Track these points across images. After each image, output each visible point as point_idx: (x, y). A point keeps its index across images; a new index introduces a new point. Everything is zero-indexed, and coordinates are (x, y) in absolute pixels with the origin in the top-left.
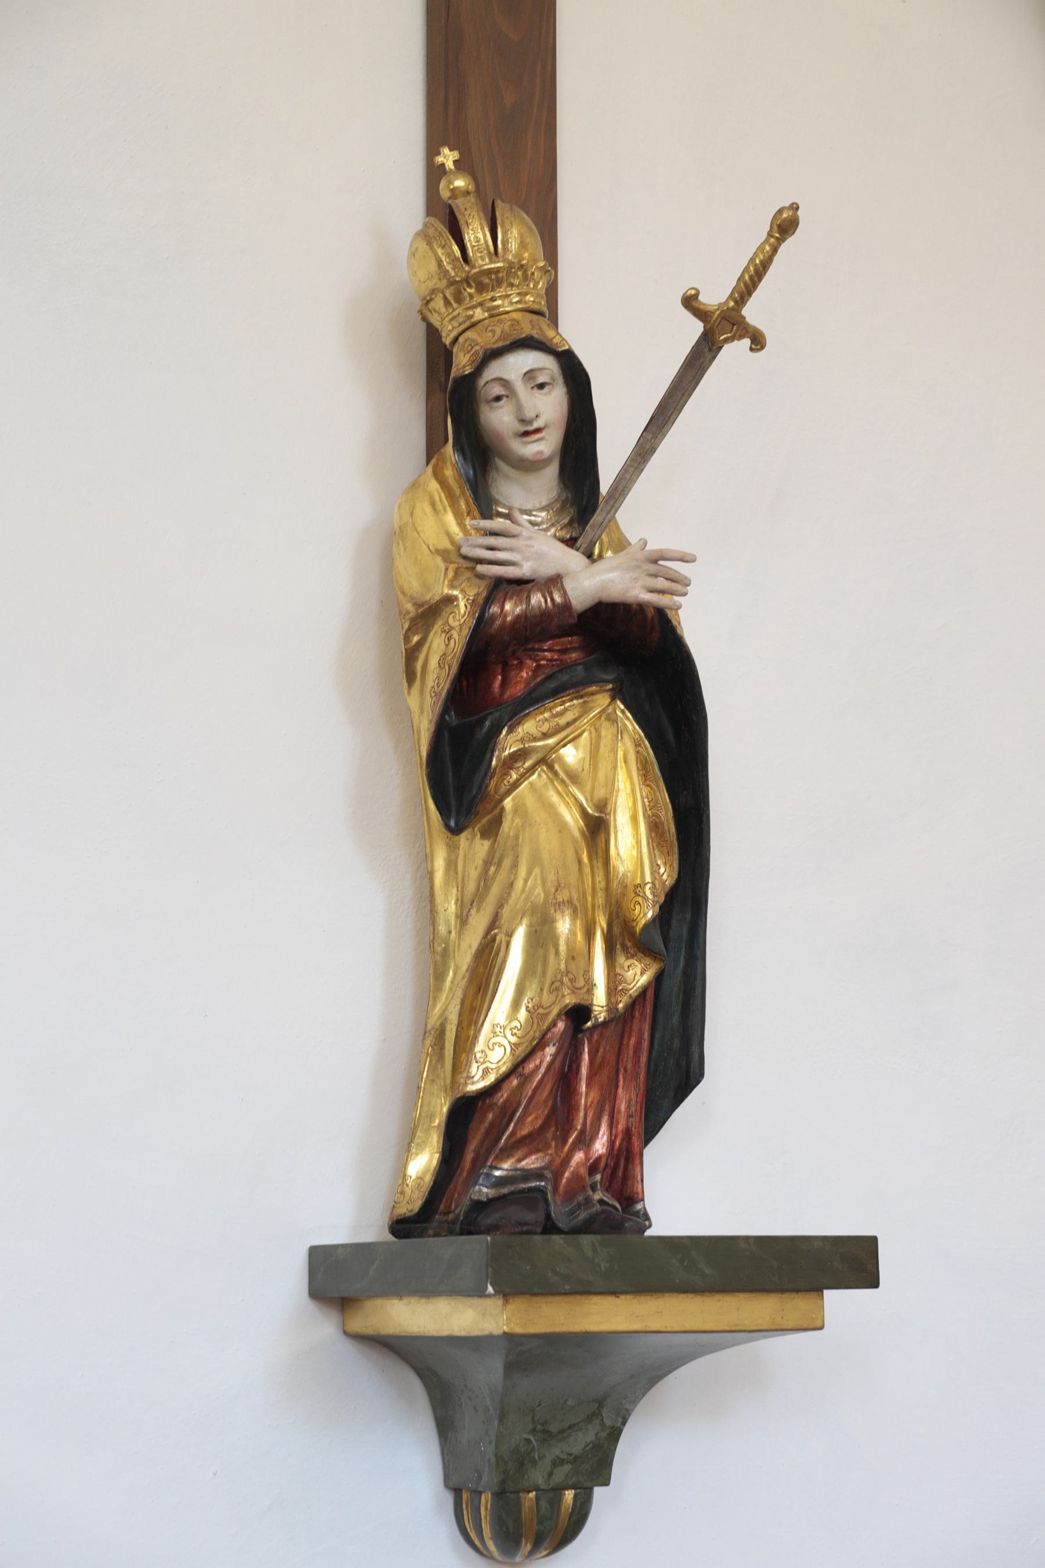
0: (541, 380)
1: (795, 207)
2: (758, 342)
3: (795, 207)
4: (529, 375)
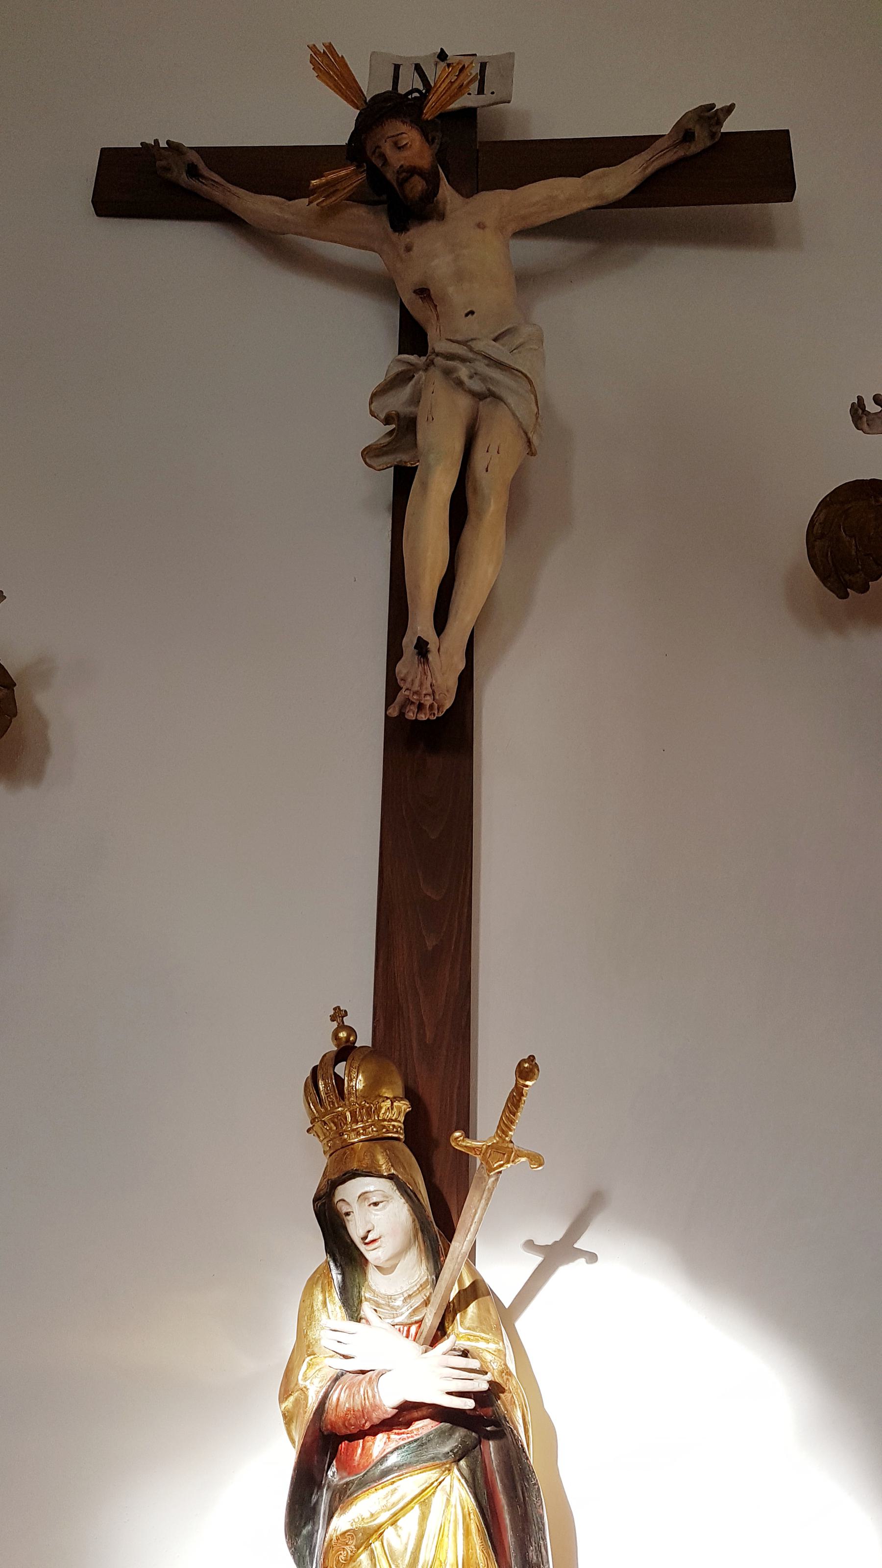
0: (375, 1200)
1: (531, 1058)
2: (536, 1159)
3: (531, 1058)
4: (363, 1196)
